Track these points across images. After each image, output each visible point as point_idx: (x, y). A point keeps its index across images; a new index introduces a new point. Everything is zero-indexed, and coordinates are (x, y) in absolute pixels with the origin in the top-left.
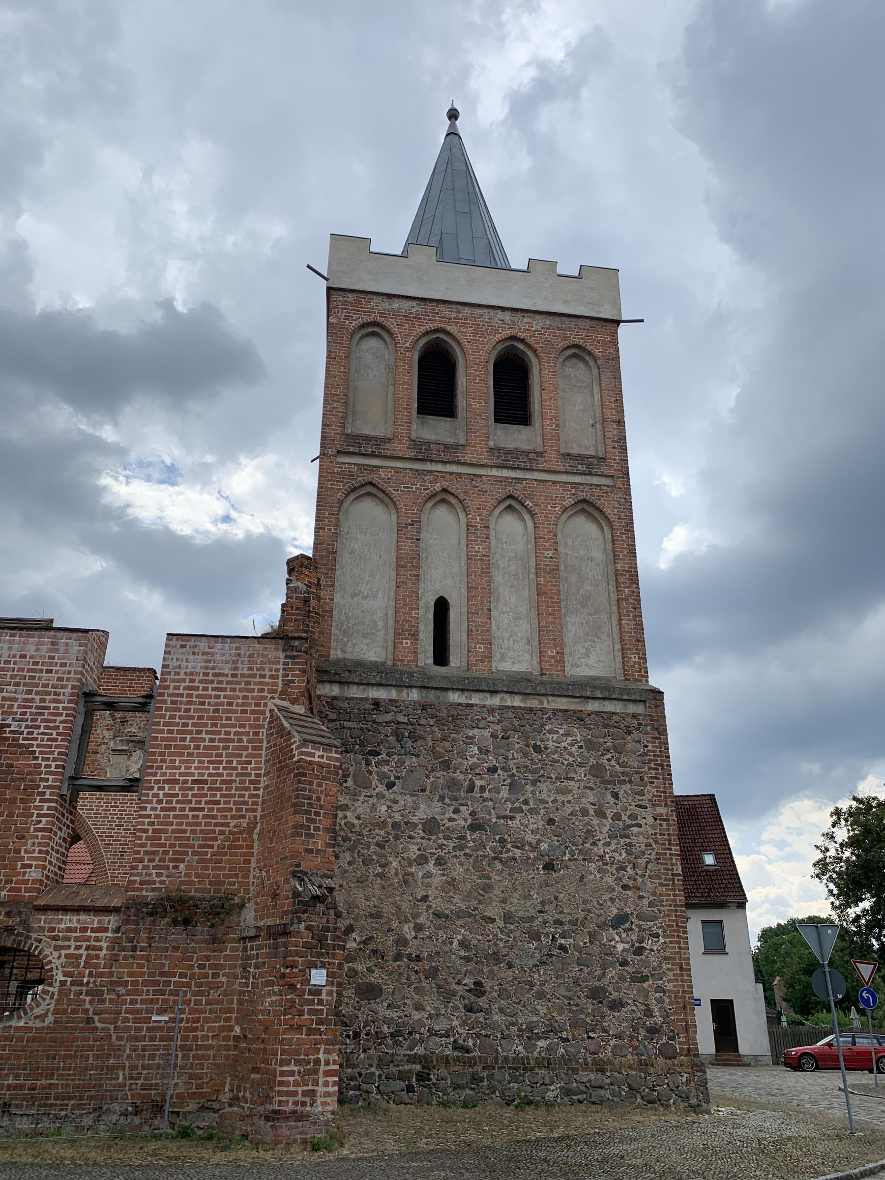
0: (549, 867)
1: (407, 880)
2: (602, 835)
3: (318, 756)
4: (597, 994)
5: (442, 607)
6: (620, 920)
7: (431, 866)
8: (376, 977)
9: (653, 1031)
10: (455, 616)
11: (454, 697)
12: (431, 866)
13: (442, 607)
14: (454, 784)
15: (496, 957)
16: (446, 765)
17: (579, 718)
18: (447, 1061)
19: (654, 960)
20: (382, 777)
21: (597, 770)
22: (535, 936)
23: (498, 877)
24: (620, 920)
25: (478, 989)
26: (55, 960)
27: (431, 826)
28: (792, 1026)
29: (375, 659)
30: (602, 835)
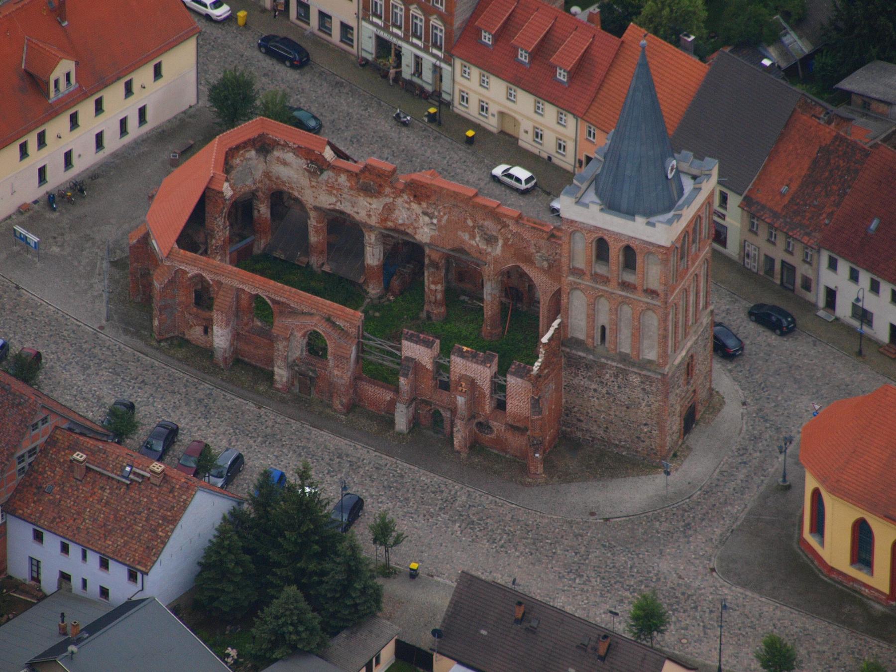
0: (628, 408)
1: (589, 400)
2: (644, 405)
3: (536, 417)
4: (638, 438)
5: (603, 328)
6: (646, 425)
7: (595, 399)
8: (582, 418)
9: (652, 449)
10: (607, 332)
11: (603, 360)
12: (595, 399)
13: (603, 328)
14: (602, 382)
15: (612, 423)
16: (600, 377)
17: (640, 374)
18: (598, 439)
19: (654, 435)
20: (582, 375)
21: (644, 389)
22: (623, 421)
23: (614, 407)
24: (646, 425)
25: (607, 428)
26: (495, 429)
27: (595, 390)
28: (167, 459)
29: (449, 600)
30: (644, 405)
